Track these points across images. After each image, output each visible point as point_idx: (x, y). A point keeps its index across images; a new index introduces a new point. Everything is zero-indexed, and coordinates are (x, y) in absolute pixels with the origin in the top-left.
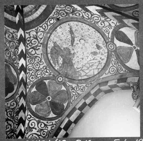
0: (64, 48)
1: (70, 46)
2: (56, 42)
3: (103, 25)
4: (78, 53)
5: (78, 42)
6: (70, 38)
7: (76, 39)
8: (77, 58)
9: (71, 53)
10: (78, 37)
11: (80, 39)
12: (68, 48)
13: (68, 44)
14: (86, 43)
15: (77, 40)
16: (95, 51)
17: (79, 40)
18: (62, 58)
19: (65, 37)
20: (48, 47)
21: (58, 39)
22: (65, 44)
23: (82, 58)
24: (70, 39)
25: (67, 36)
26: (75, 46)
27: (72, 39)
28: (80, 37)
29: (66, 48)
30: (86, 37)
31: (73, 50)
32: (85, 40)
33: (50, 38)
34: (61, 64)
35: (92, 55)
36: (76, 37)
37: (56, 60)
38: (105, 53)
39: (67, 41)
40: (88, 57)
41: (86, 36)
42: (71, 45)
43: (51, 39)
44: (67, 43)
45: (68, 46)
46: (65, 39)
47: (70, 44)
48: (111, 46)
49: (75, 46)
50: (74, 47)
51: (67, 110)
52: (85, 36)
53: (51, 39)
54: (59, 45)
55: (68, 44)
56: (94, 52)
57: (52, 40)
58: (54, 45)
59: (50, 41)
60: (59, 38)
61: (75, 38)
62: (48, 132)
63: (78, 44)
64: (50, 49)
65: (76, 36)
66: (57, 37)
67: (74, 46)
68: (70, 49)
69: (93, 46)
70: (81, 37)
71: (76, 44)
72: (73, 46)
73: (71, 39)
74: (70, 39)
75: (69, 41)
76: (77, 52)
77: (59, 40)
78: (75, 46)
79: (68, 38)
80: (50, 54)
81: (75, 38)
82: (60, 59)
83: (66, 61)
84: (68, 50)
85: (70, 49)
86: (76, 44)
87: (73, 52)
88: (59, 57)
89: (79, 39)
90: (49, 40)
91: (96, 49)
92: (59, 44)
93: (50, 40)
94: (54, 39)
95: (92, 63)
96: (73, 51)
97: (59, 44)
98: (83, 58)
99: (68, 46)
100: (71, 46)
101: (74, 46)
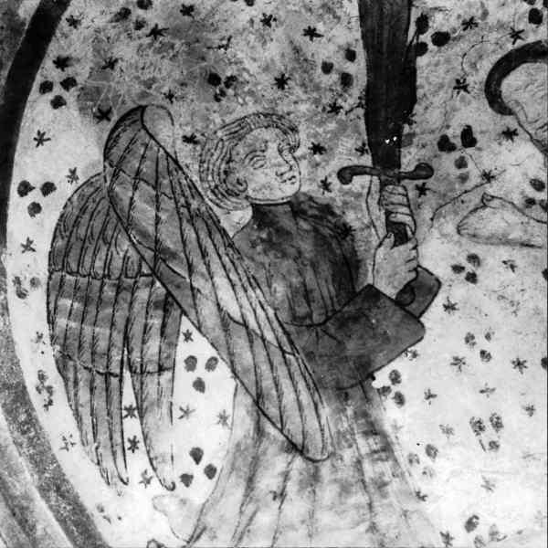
0: (262, 214)
1: (346, 175)
2: (142, 109)
4: (472, 278)
5: (475, 113)
6: (351, 56)
7: (431, 69)
8: (472, 356)
9: (373, 294)
10: (469, 24)
11: (505, 66)
12: (327, 209)
13: (317, 149)
17: (477, 78)
18: (223, 369)
19: (278, 32)
20: (25, 189)
21: (168, 72)
22: (273, 147)
24: (346, 80)
25: (311, 33)
26: (424, 170)
27: (372, 67)
29: (296, 207)
31: (400, 234)
33: (54, 50)
34: (210, 471)
36: (441, 39)
37: (129, 399)
39: (299, 105)
40: (489, 431)
42: (367, 160)
43: (62, 63)
44: (304, 138)
45: (325, 185)
46: (279, 66)
47: (347, 151)
50: (411, 185)
51: (216, 216)
53: (62, 63)
54: (185, 154)
55: (317, 149)
57: (82, 72)
58: (106, 156)
59: (46, 87)
60: (195, 51)
61: (422, 61)
63: (468, 138)
64: (50, 217)
65: (438, 23)
66: (156, 32)
67: (412, 176)
68: (351, 218)
71: (445, 145)
72: (400, 178)
73: (358, 69)
74: (346, 80)
75: (335, 109)
77: (191, 92)
78: (424, 170)
79: (323, 51)
80: (37, 298)
81: (422, 49)
82: (199, 385)
83: (294, 426)
84: (321, 241)
85: (346, 231)
86: (445, 145)
87: (405, 276)
88: (183, 350)
89: (486, 66)
90: (39, 79)
92: (189, 140)
93: (48, 71)
94: (111, 64)
96: (404, 249)
97: (189, 140)
99: (325, 185)
100: (359, 182)
101: (412, 176)
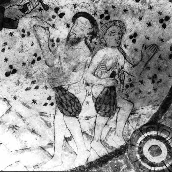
3: (40, 84)
4: (23, 36)
11: (85, 15)
14: (86, 43)
15: (75, 6)
16: (81, 96)
17: (79, 9)
23: (11, 67)
28: (96, 8)
30: (112, 34)
32: (94, 35)
35: (53, 100)
38: (103, 142)
41: (113, 28)
48: (156, 151)
49: (44, 12)
52: (115, 23)
56: (74, 98)
62: (151, 48)
63: (62, 15)
69: (95, 78)
70: (98, 14)
76: (23, 31)
87: (13, 17)
91: (90, 99)
95: (19, 119)
98: (15, 71)
